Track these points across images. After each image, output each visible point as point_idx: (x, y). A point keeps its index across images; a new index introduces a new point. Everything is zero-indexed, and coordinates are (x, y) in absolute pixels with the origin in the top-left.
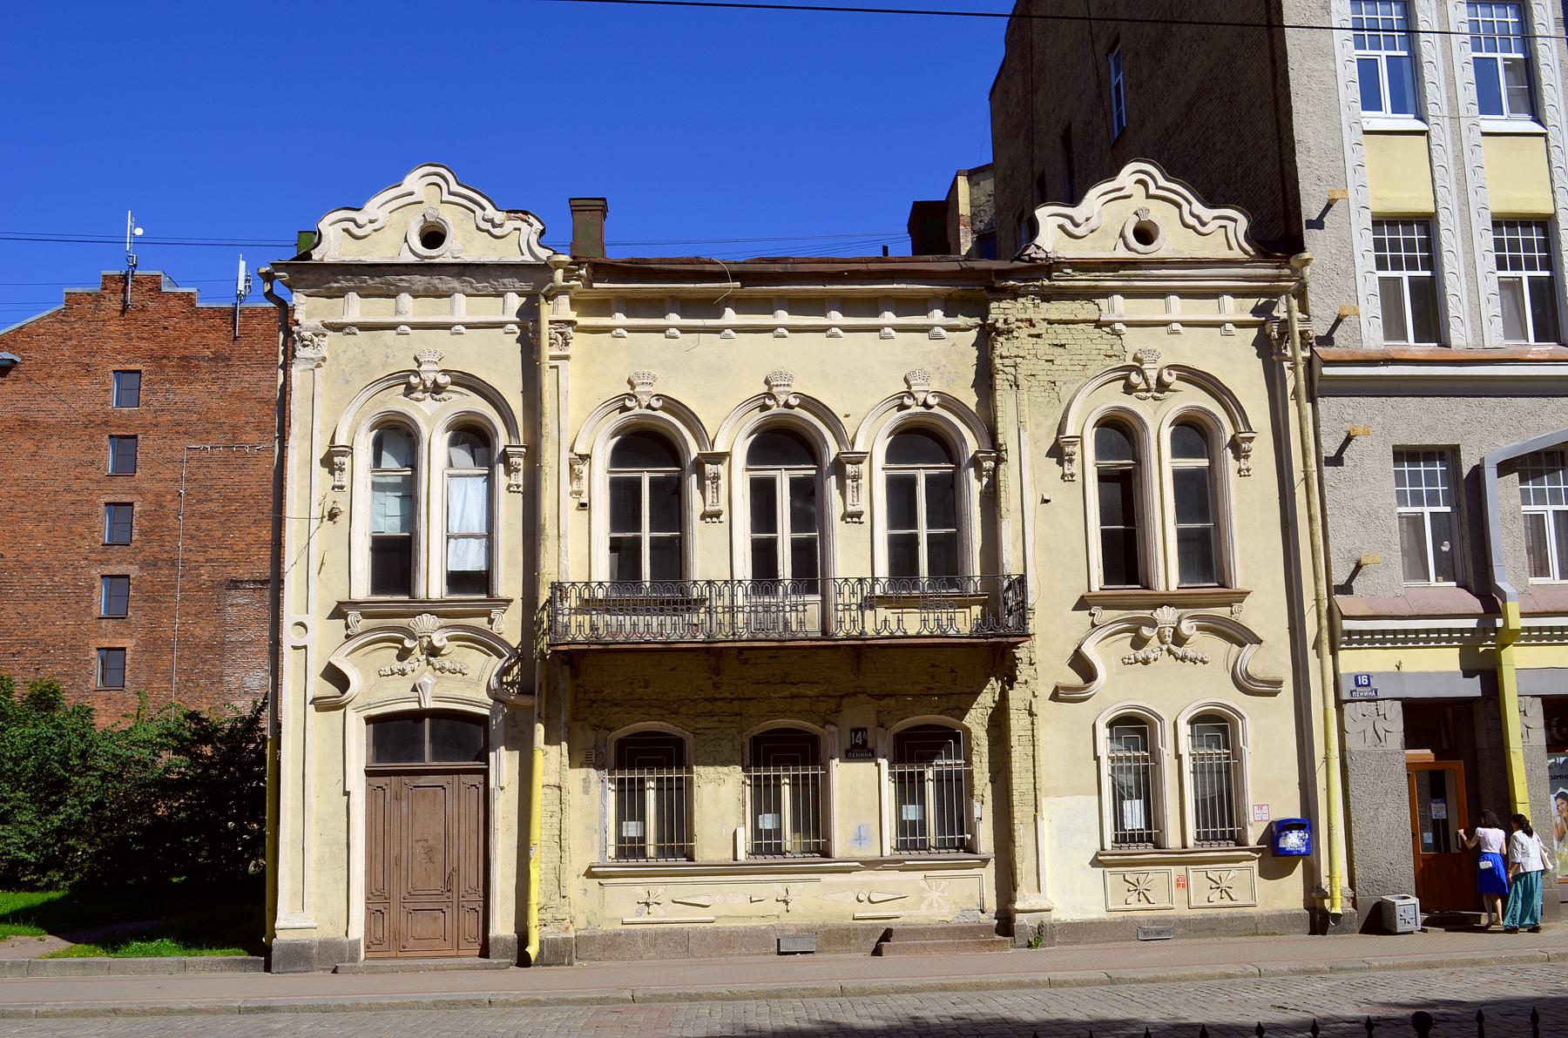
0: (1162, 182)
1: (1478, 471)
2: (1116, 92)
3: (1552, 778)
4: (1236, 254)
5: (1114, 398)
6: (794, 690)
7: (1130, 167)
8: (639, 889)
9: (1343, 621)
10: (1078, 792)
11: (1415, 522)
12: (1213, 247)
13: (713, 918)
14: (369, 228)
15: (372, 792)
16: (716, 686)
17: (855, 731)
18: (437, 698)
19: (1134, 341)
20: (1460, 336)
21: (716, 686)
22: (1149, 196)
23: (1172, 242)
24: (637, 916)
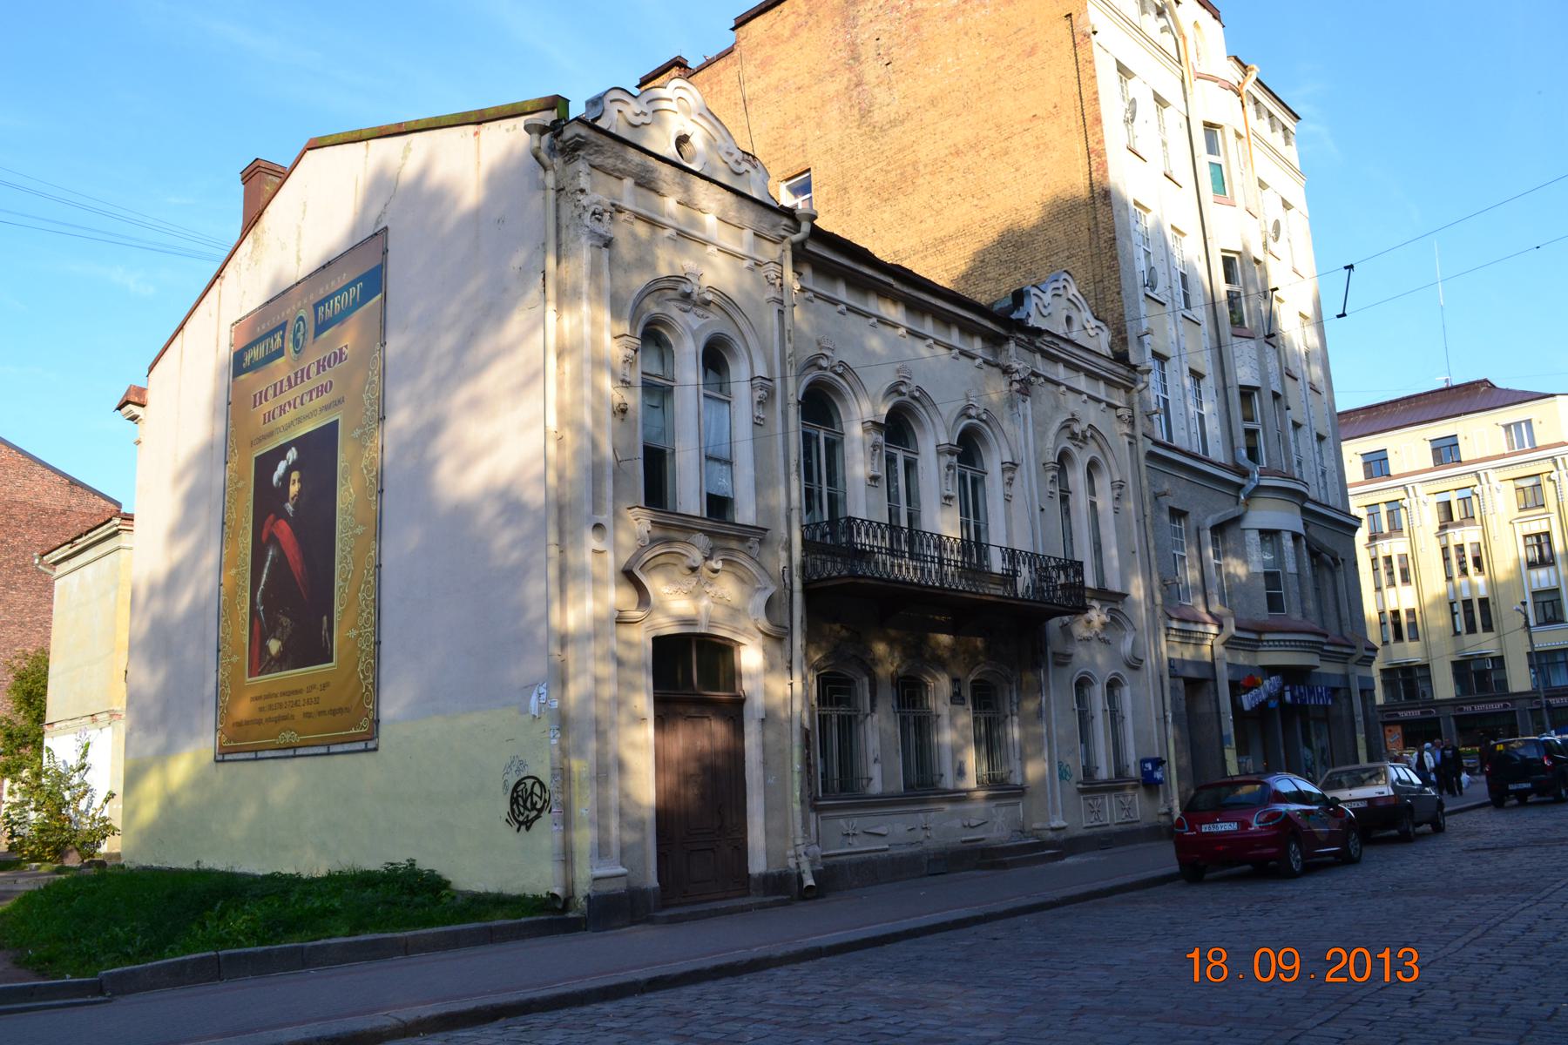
8: (842, 822)
13: (887, 847)
24: (841, 848)
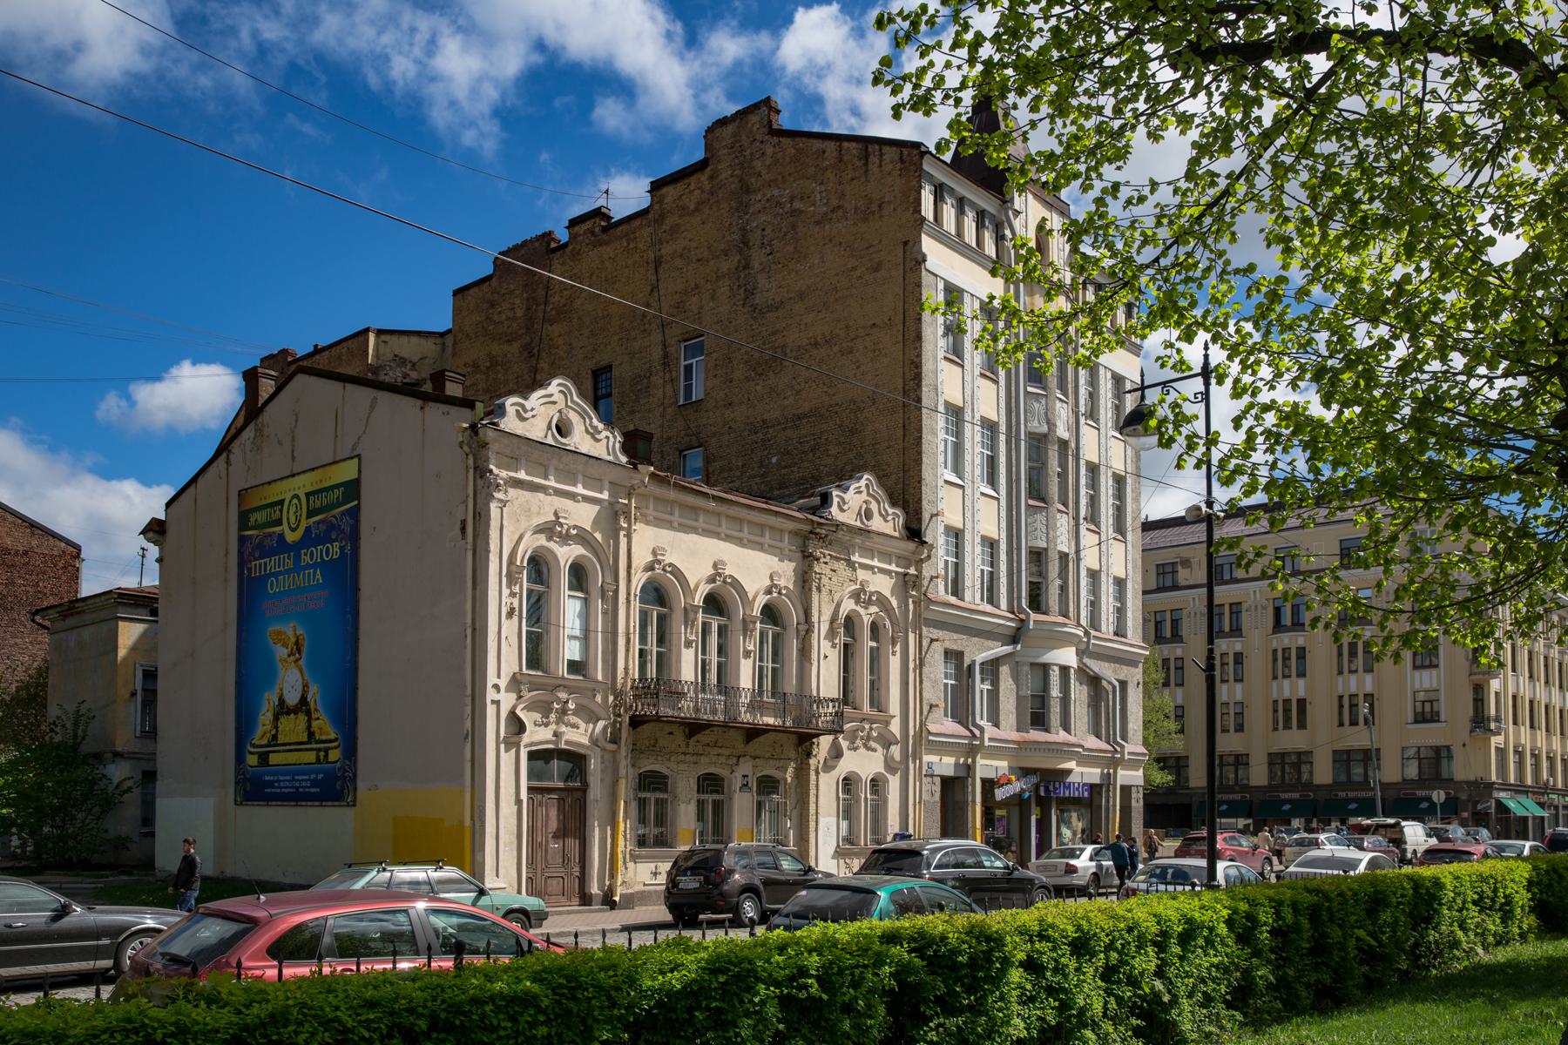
0: (575, 398)
1: (971, 668)
2: (1060, 489)
3: (156, 676)
4: (897, 534)
5: (848, 605)
6: (720, 751)
7: (555, 382)
9: (151, 580)
10: (830, 816)
11: (946, 685)
12: (599, 450)
14: (529, 414)
15: (530, 799)
16: (687, 745)
17: (744, 776)
18: (567, 742)
19: (862, 574)
20: (968, 595)
21: (687, 745)
22: (567, 406)
23: (580, 440)
